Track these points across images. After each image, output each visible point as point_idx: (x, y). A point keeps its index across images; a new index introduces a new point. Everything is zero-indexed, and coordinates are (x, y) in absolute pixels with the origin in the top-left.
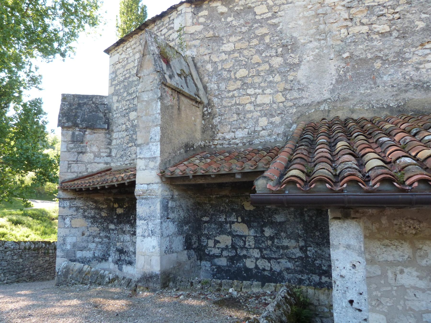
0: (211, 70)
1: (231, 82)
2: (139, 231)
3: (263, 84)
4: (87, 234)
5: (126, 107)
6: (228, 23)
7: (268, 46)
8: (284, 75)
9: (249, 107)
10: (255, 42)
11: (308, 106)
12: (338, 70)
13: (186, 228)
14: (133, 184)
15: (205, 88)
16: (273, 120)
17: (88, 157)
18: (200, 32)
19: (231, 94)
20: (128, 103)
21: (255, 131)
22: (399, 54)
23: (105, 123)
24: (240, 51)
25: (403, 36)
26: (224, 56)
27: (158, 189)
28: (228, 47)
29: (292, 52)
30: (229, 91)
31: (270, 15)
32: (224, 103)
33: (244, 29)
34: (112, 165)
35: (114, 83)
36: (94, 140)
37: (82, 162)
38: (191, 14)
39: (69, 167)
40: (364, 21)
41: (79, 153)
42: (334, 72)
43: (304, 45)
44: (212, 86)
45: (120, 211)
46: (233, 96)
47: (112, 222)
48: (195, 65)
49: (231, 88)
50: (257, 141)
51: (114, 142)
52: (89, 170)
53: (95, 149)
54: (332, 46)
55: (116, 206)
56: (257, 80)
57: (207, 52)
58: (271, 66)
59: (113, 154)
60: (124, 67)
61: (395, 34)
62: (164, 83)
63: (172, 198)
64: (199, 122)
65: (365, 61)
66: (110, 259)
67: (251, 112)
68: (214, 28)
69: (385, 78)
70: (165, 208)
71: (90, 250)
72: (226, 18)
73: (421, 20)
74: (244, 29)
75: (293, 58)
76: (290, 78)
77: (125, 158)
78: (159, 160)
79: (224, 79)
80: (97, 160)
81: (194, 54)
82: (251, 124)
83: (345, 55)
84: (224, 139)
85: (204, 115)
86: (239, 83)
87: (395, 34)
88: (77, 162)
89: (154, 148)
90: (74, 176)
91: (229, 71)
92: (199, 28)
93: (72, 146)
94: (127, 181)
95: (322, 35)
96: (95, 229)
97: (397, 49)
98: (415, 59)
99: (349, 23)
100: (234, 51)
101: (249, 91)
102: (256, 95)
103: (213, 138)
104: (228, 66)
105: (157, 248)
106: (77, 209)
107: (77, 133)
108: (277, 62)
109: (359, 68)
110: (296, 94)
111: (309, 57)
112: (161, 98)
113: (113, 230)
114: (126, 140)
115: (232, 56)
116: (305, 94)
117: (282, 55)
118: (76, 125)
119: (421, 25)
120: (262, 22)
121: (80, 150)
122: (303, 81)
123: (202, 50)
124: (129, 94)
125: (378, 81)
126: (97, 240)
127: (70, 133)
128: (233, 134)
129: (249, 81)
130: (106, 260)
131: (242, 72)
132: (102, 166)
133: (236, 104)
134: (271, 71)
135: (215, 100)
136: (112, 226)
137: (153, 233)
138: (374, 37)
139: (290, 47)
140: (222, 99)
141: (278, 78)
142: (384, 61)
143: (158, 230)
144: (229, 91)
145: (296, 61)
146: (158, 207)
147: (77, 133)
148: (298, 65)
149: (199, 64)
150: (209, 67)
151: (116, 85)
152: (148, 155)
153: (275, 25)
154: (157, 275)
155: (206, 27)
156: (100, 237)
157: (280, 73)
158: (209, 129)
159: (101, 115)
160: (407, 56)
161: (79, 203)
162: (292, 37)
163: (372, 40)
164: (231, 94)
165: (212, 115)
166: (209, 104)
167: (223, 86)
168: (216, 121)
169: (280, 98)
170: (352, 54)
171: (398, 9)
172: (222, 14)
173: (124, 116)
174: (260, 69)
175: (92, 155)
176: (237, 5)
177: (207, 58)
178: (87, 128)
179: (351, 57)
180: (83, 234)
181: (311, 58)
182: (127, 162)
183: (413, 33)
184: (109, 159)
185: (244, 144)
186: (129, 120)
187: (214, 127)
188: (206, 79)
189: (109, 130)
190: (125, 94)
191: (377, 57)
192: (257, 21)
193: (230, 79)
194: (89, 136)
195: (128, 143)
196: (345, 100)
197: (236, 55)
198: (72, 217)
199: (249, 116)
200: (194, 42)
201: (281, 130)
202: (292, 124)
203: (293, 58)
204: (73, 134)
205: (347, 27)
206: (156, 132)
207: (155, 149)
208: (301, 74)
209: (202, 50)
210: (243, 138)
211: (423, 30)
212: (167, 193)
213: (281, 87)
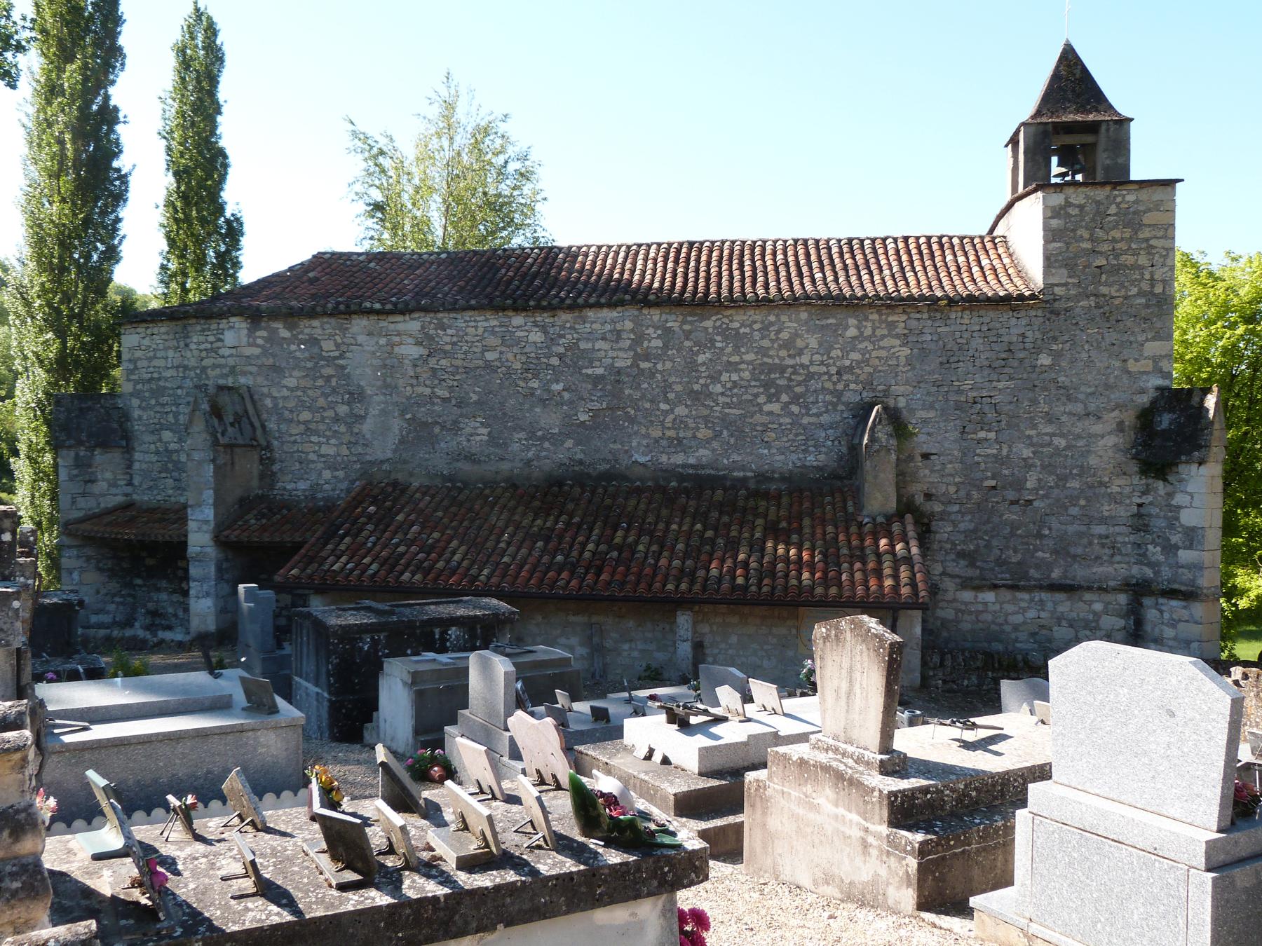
0: (270, 406)
1: (293, 425)
2: (192, 592)
3: (327, 433)
4: (103, 591)
5: (156, 421)
6: (291, 353)
7: (334, 391)
8: (350, 426)
9: (312, 457)
10: (320, 382)
11: (372, 463)
12: (401, 430)
13: (111, 77)
14: (184, 545)
15: (263, 427)
16: (337, 473)
17: (100, 487)
18: (258, 357)
19: (293, 438)
20: (158, 416)
21: (318, 484)
22: (455, 422)
23: (122, 438)
24: (304, 389)
25: (459, 405)
26: (285, 393)
27: (212, 551)
28: (291, 382)
29: (359, 402)
30: (291, 435)
31: (337, 354)
32: (285, 448)
33: (309, 365)
34: (135, 497)
35: (133, 377)
36: (106, 465)
37: (91, 494)
38: (245, 332)
39: (73, 503)
40: (428, 382)
41: (87, 482)
42: (397, 432)
43: (371, 396)
44: (272, 425)
45: (150, 562)
46: (295, 442)
47: (139, 576)
48: (251, 397)
49: (294, 431)
50: (319, 495)
51: (137, 466)
52: (102, 505)
53: (108, 475)
54: (397, 404)
55: (144, 554)
56: (322, 427)
57: (265, 383)
58: (336, 414)
59: (136, 482)
60: (150, 359)
61: (454, 402)
62: (216, 443)
63: (227, 560)
64: (256, 468)
65: (426, 424)
66: (137, 624)
67: (313, 462)
68: (274, 356)
69: (442, 445)
70: (219, 569)
71: (108, 612)
72: (289, 345)
73: (474, 392)
74: (309, 365)
75: (359, 409)
76: (356, 430)
77: (155, 492)
78: (212, 525)
79: (285, 420)
80: (114, 490)
81: (251, 383)
82: (313, 477)
83: (408, 416)
84: (285, 489)
85: (261, 459)
86: (302, 427)
87: (454, 402)
88: (84, 494)
89: (207, 511)
90: (80, 514)
91: (291, 411)
92: (257, 351)
93: (75, 472)
94: (176, 539)
95: (388, 388)
96: (114, 586)
97: (454, 417)
98: (468, 430)
99: (414, 382)
100: (297, 388)
101: (313, 439)
102: (320, 444)
103: (272, 488)
104: (291, 405)
105: (213, 609)
106: (88, 559)
107: (82, 454)
108: (343, 410)
109: (421, 432)
110: (360, 450)
111: (374, 411)
112: (213, 461)
113: (140, 586)
114: (157, 466)
115: (295, 393)
116: (369, 450)
117: (348, 404)
118: (80, 443)
119: (474, 397)
120: (330, 361)
121: (87, 478)
122: (368, 436)
123: (260, 380)
124: (158, 404)
125: (437, 446)
126: (118, 599)
127: (72, 454)
128: (293, 485)
129: (313, 426)
130: (132, 626)
131: (306, 416)
132: (120, 499)
133: (298, 451)
134: (337, 419)
135: (275, 443)
136: (139, 581)
137: (208, 594)
138: (436, 400)
139: (357, 396)
140: (283, 443)
141: (343, 429)
142: (443, 428)
143: (212, 591)
144: (291, 435)
145: (362, 413)
146: (212, 569)
147: (82, 454)
148: (363, 417)
149: (256, 397)
150: (268, 402)
151: (136, 382)
152: (200, 518)
153: (343, 367)
154: (212, 634)
155: (265, 352)
156: (122, 596)
157: (346, 423)
158: (268, 477)
159: (115, 425)
160: (461, 425)
161: (89, 551)
162: (359, 386)
163: (433, 404)
164: (293, 438)
165: (272, 461)
166: (268, 447)
167: (283, 427)
168: (276, 467)
169: (344, 451)
170: (414, 415)
171: (457, 377)
172: (284, 339)
173: (152, 432)
174: (325, 414)
175: (105, 485)
176: (302, 332)
177: (265, 390)
178: (96, 446)
179: (413, 419)
180: (98, 592)
181: (377, 412)
182: (159, 498)
183: (468, 405)
184: (129, 489)
185: (306, 497)
186: (160, 440)
187: (273, 474)
188: (265, 416)
189: (129, 450)
190: (153, 402)
191: (438, 423)
192: (323, 358)
193: (291, 421)
194: (99, 457)
195: (160, 472)
196: (405, 462)
197: (299, 393)
198: (82, 570)
199: (312, 466)
200: (250, 368)
201: (344, 486)
202: (355, 481)
203: (359, 409)
204: (77, 455)
205: (412, 386)
206: (209, 495)
207: (209, 513)
208: (367, 427)
209: (260, 380)
210: (305, 490)
211: (475, 403)
212: (221, 556)
213: (346, 438)
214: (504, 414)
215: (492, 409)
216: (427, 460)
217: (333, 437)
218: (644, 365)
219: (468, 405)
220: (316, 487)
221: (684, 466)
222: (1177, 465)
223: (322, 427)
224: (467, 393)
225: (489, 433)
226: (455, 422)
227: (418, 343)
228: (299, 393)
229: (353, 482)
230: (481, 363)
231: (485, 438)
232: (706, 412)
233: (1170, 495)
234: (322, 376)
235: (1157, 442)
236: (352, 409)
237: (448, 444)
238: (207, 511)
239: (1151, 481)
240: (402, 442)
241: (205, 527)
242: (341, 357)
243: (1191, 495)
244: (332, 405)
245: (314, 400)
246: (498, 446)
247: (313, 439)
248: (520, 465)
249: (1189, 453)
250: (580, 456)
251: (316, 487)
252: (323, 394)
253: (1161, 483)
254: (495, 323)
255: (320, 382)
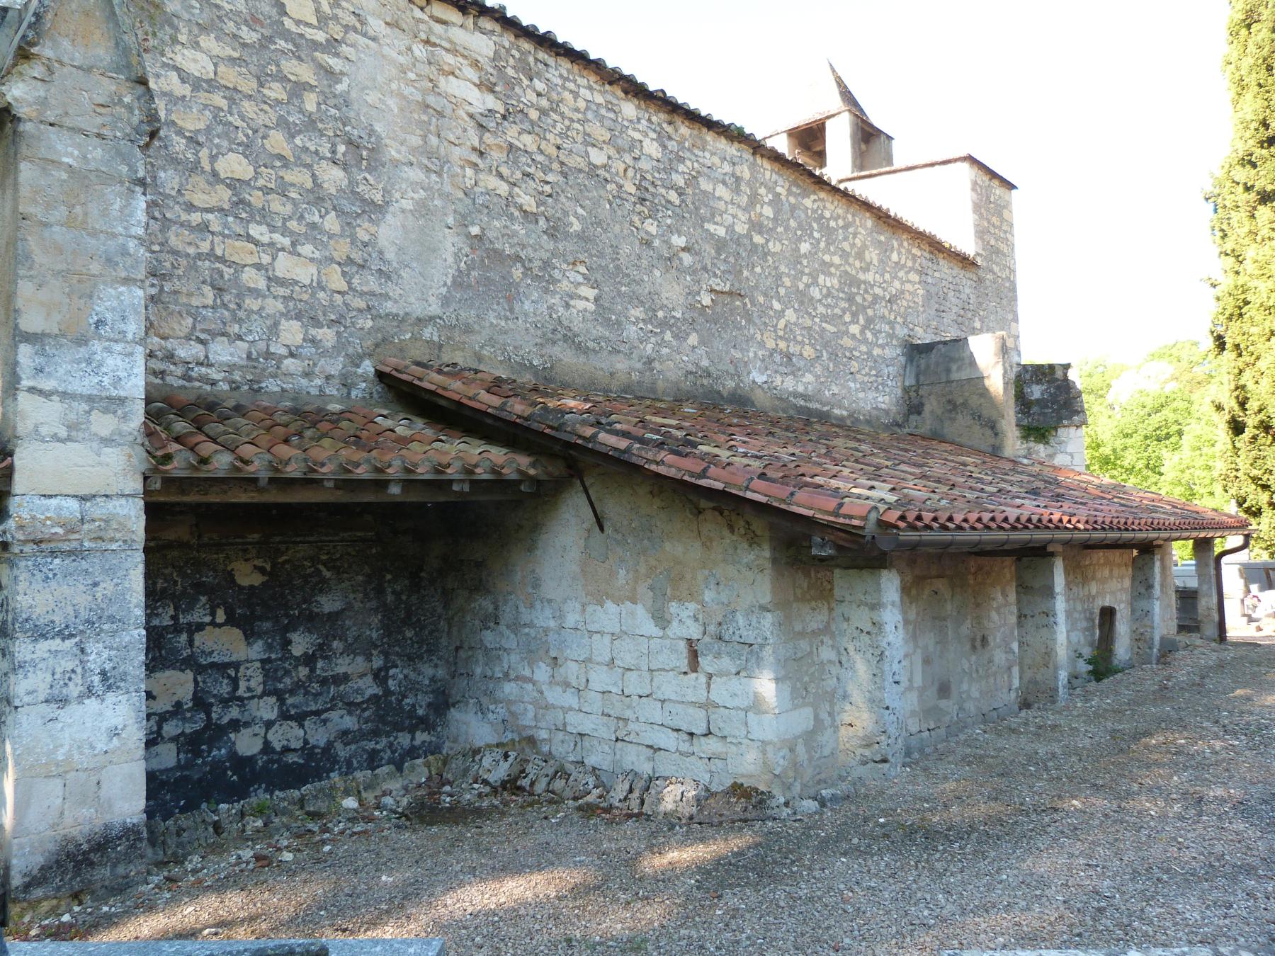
1: (199, 180)
7: (311, 124)
9: (251, 278)
10: (275, 91)
19: (196, 218)
21: (268, 355)
24: (233, 94)
29: (370, 169)
30: (190, 207)
31: (320, 37)
33: (248, 36)
43: (396, 164)
46: (204, 228)
49: (199, 199)
50: (272, 385)
56: (278, 206)
65: (497, 255)
67: (255, 293)
69: (527, 306)
76: (363, 235)
82: (257, 329)
83: (475, 230)
89: (113, 363)
91: (193, 141)
97: (545, 256)
100: (212, 85)
101: (256, 231)
108: (333, 177)
110: (373, 284)
119: (577, 227)
122: (390, 255)
131: (234, 165)
134: (317, 196)
139: (361, 152)
141: (331, 223)
144: (190, 207)
145: (378, 198)
152: (85, 385)
157: (341, 213)
160: (557, 274)
162: (372, 133)
164: (196, 218)
181: (407, 204)
191: (518, 258)
196: (468, 330)
199: (252, 303)
201: (335, 366)
202: (361, 357)
208: (388, 233)
210: (232, 367)
213: (342, 249)
214: (618, 268)
215: (601, 255)
216: (505, 332)
217: (308, 238)
218: (758, 239)
219: (567, 236)
220: (262, 360)
221: (796, 394)
222: (1056, 429)
223: (278, 206)
224: (566, 213)
225: (596, 300)
226: (546, 264)
227: (487, 86)
228: (219, 100)
229: (356, 361)
230: (583, 165)
231: (591, 307)
232: (809, 323)
233: (1051, 456)
234: (284, 79)
235: (1035, 409)
236: (353, 183)
237: (532, 304)
238: (113, 363)
239: (1032, 444)
240: (459, 282)
241: (103, 424)
242: (332, 45)
243: (1071, 455)
244: (305, 160)
245: (259, 132)
246: (607, 323)
247: (256, 231)
248: (639, 366)
249: (1070, 418)
250: (705, 363)
251: (262, 360)
252: (282, 123)
253: (1041, 446)
254: (599, 99)
255: (275, 91)
